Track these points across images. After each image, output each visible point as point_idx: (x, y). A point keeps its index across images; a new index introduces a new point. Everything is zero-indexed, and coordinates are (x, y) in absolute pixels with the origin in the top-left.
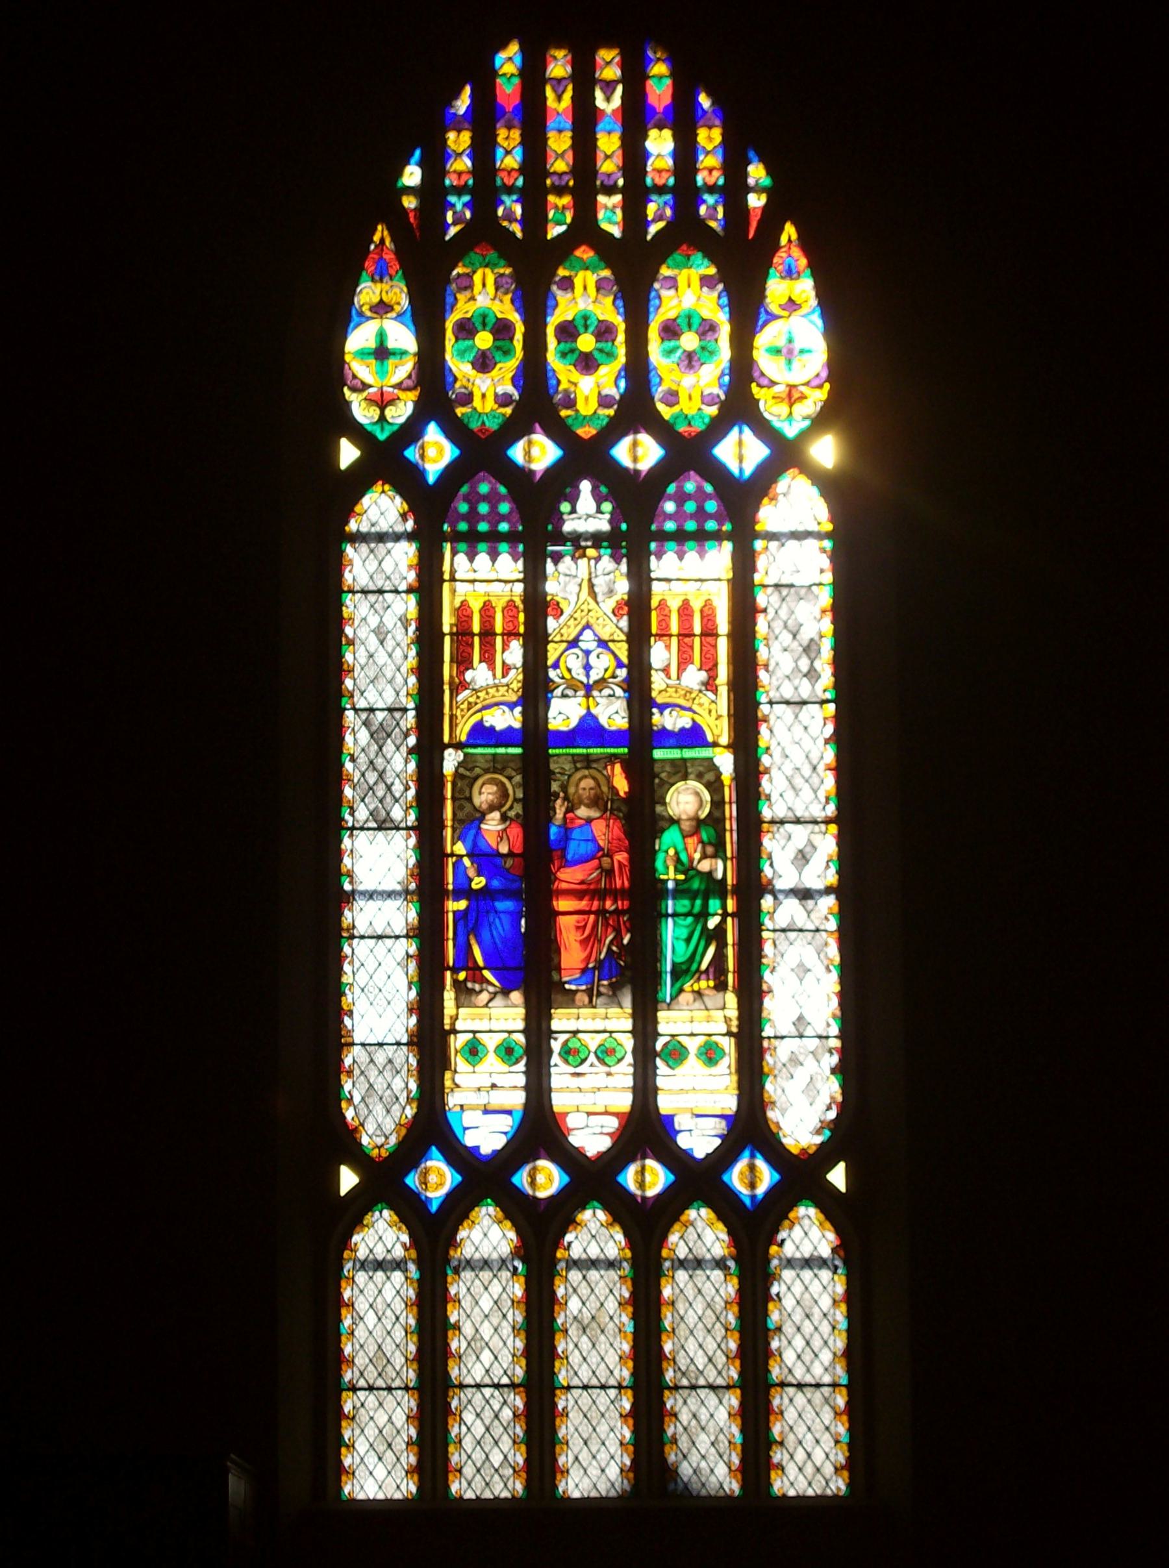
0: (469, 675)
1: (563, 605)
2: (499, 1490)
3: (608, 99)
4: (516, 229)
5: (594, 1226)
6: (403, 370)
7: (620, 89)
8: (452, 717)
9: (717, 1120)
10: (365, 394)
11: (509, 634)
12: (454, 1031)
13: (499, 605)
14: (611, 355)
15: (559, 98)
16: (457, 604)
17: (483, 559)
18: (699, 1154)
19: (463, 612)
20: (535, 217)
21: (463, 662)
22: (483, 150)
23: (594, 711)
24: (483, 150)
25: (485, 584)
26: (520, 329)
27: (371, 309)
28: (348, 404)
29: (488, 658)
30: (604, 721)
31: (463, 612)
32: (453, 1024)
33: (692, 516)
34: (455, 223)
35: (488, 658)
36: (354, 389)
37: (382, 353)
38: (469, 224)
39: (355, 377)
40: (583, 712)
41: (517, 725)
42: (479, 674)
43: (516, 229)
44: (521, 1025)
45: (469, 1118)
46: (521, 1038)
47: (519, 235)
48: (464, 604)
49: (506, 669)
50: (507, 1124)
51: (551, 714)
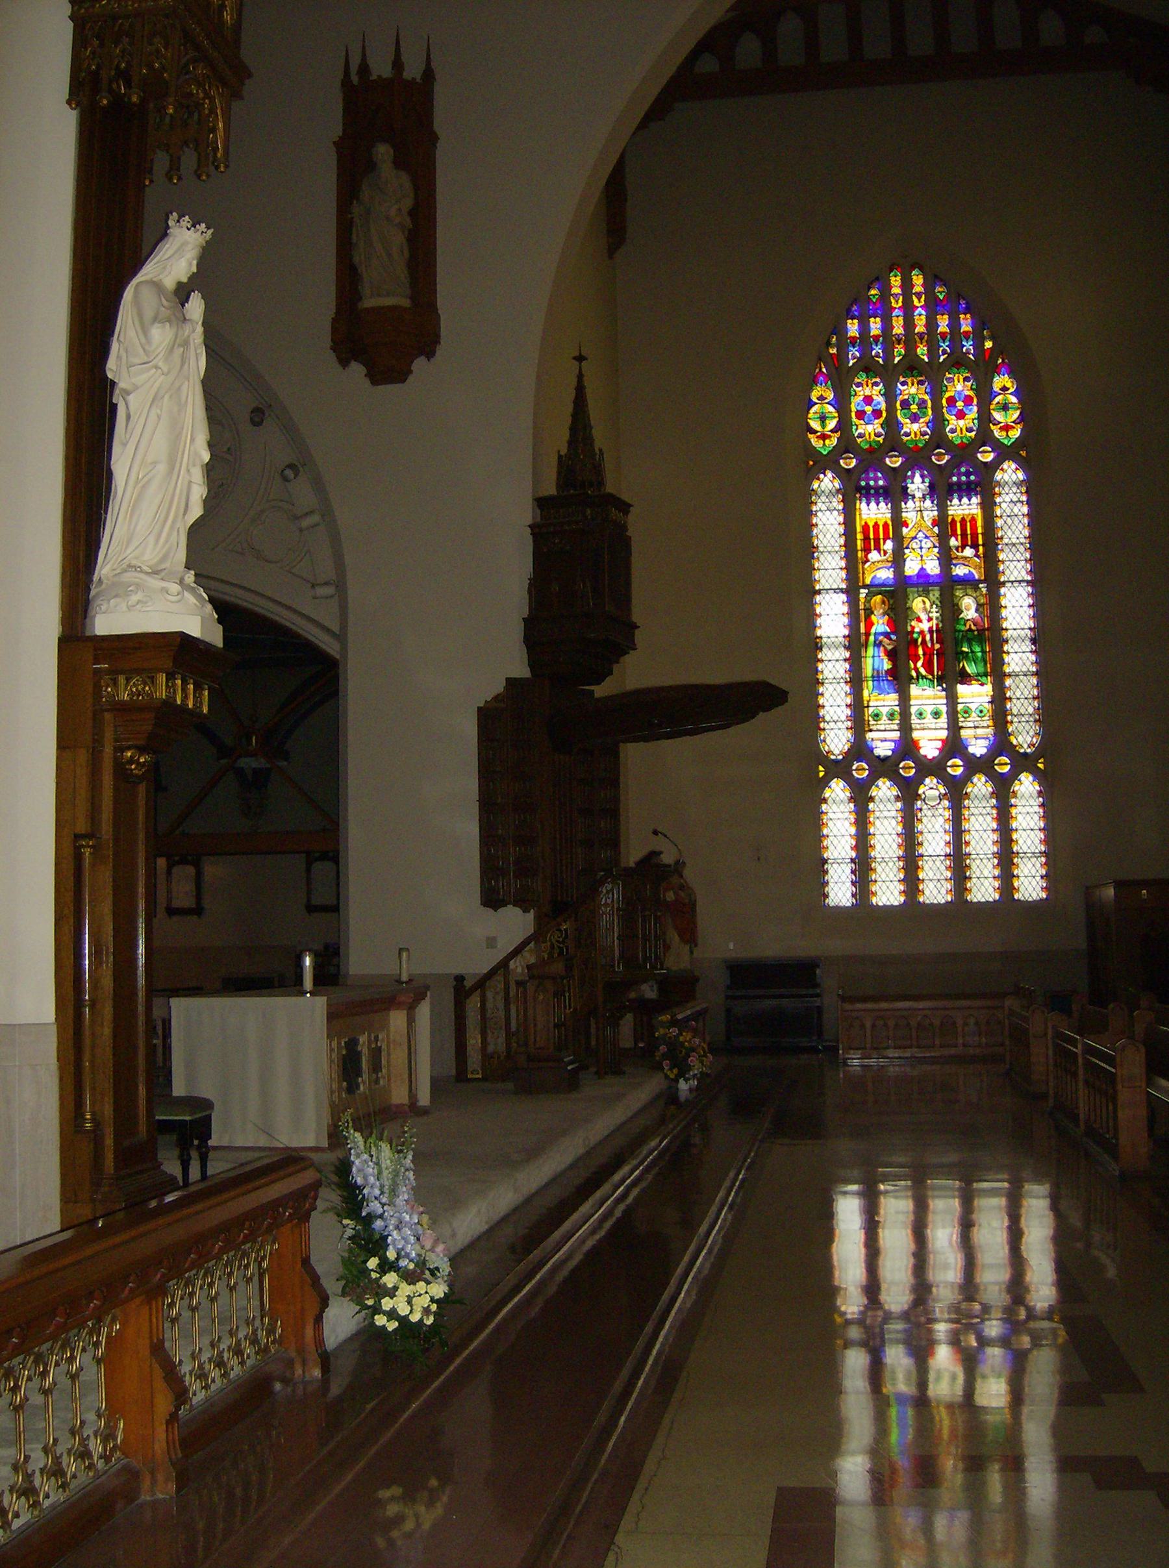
0: (870, 556)
1: (909, 522)
2: (1035, 897)
3: (920, 301)
4: (881, 361)
5: (979, 784)
6: (831, 424)
7: (901, 298)
8: (222, 593)
9: (983, 740)
10: (999, 426)
11: (886, 538)
12: (868, 706)
13: (881, 524)
14: (925, 414)
15: (897, 302)
16: (863, 523)
17: (873, 504)
18: (930, 757)
19: (866, 528)
20: (888, 354)
21: (867, 550)
22: (909, 324)
23: (924, 567)
24: (909, 324)
25: (112, 542)
26: (929, 404)
27: (818, 399)
28: (992, 431)
29: (878, 548)
30: (929, 571)
31: (866, 528)
32: (868, 703)
33: (868, 484)
34: (943, 355)
35: (878, 548)
36: (994, 425)
37: (823, 418)
38: (859, 359)
39: (995, 419)
40: (920, 567)
41: (891, 576)
42: (874, 556)
43: (881, 361)
44: (897, 703)
45: (874, 744)
46: (897, 709)
47: (926, 360)
48: (866, 523)
49: (885, 553)
50: (985, 743)
51: (906, 569)
